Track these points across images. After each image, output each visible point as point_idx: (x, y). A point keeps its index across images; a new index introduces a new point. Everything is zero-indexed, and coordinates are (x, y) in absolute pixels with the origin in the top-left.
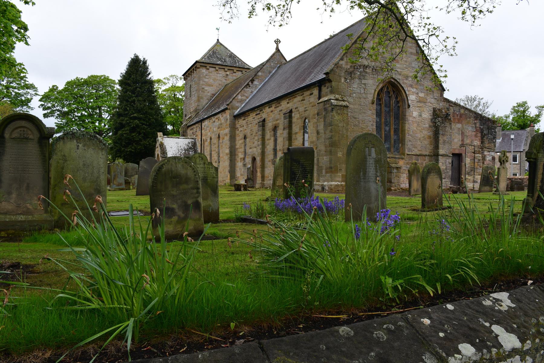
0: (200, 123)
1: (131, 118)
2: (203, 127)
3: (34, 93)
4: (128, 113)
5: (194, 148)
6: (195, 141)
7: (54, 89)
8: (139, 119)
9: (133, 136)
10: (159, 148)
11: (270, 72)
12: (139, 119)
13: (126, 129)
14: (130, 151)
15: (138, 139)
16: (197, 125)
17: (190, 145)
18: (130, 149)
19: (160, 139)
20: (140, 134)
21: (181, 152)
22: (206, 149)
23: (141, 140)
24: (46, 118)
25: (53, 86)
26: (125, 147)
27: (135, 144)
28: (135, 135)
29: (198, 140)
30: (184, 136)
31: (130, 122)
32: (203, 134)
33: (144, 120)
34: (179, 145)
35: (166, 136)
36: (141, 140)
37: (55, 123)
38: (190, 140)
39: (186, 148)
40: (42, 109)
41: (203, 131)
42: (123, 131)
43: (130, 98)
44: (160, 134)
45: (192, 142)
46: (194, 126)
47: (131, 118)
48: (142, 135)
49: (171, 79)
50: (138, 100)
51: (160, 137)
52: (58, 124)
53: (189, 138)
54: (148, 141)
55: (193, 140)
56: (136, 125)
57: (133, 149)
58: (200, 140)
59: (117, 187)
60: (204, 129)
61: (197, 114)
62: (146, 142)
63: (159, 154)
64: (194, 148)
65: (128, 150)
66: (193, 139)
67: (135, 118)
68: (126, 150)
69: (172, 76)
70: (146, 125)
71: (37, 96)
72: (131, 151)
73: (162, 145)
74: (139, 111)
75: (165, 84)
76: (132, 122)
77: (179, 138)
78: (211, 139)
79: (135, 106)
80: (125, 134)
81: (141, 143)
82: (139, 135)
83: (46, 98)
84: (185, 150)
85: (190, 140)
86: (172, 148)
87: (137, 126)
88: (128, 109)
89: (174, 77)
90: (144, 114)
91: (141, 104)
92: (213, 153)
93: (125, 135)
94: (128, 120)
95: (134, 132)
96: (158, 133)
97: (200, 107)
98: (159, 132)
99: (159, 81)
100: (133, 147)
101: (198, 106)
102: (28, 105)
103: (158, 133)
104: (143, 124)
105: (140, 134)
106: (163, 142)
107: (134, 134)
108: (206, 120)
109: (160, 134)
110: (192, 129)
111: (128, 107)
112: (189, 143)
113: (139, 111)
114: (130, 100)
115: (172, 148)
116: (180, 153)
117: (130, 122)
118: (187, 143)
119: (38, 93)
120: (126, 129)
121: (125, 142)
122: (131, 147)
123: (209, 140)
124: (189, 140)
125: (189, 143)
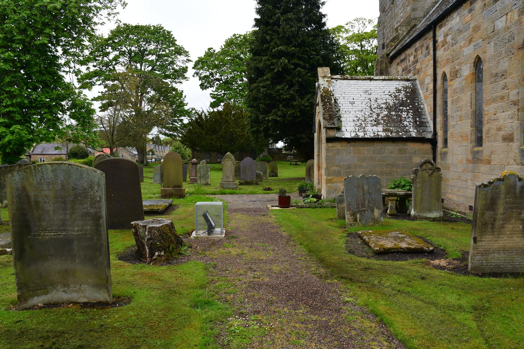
0: (431, 34)
1: (274, 56)
2: (440, 39)
3: (185, 58)
4: (269, 48)
5: (412, 103)
6: (414, 86)
7: (210, 54)
8: (290, 56)
9: (278, 91)
10: (321, 104)
11: (328, 181)
12: (290, 56)
13: (265, 78)
14: (273, 119)
15: (288, 96)
16: (418, 44)
17: (402, 95)
18: (274, 117)
19: (322, 83)
20: (291, 85)
21: (378, 115)
22: (456, 102)
23: (293, 98)
24: (205, 90)
25: (209, 49)
26: (267, 112)
27: (283, 106)
28: (283, 89)
29: (422, 83)
30: (381, 74)
31: (272, 64)
32: (439, 59)
33: (300, 58)
34: (373, 97)
35: (338, 76)
36: (293, 98)
37: (211, 94)
38: (400, 84)
39: (391, 103)
40: (198, 78)
41: (439, 53)
42: (260, 82)
43: (271, 18)
44: (323, 71)
45: (407, 87)
46: (408, 52)
47: (274, 56)
48: (296, 87)
49: (356, 24)
50: (287, 20)
51: (324, 77)
52: (214, 95)
53: (397, 80)
54: (308, 100)
55: (407, 84)
56: (282, 68)
57: (279, 116)
58: (429, 80)
59: (145, 241)
60: (445, 42)
61: (411, 29)
62: (303, 102)
63: (322, 119)
64: (412, 103)
65: (270, 118)
66: (408, 80)
67: (281, 54)
68: (267, 118)
69: (356, 20)
70: (304, 68)
71: (190, 62)
72: (275, 121)
73: (328, 96)
74: (288, 40)
75: (347, 31)
76: (277, 63)
77: (371, 80)
78: (478, 62)
79: (280, 30)
80: (263, 87)
81: (295, 103)
82: (290, 88)
83: (200, 63)
84: (389, 108)
85: (400, 84)
86: (353, 103)
87: (285, 69)
88: (268, 37)
89: (361, 22)
90: (300, 45)
91: (292, 27)
92: (489, 109)
93: (262, 89)
94: (268, 60)
95: (280, 83)
96: (320, 70)
97: (419, 14)
98: (321, 66)
99: (339, 29)
100: (279, 113)
101: (414, 10)
102: (184, 76)
103: (320, 70)
104: (296, 65)
105: (291, 85)
106: (331, 89)
107: (279, 87)
108: (455, 15)
109: (323, 71)
110: (402, 61)
111: (269, 34)
112: (399, 91)
113: (288, 40)
114: (271, 21)
115: (353, 103)
116: (375, 116)
117: (272, 64)
118: (393, 90)
119: (189, 58)
120: (265, 78)
121: (265, 104)
122: (276, 113)
123: (467, 70)
124: (397, 83)
125: (399, 91)
